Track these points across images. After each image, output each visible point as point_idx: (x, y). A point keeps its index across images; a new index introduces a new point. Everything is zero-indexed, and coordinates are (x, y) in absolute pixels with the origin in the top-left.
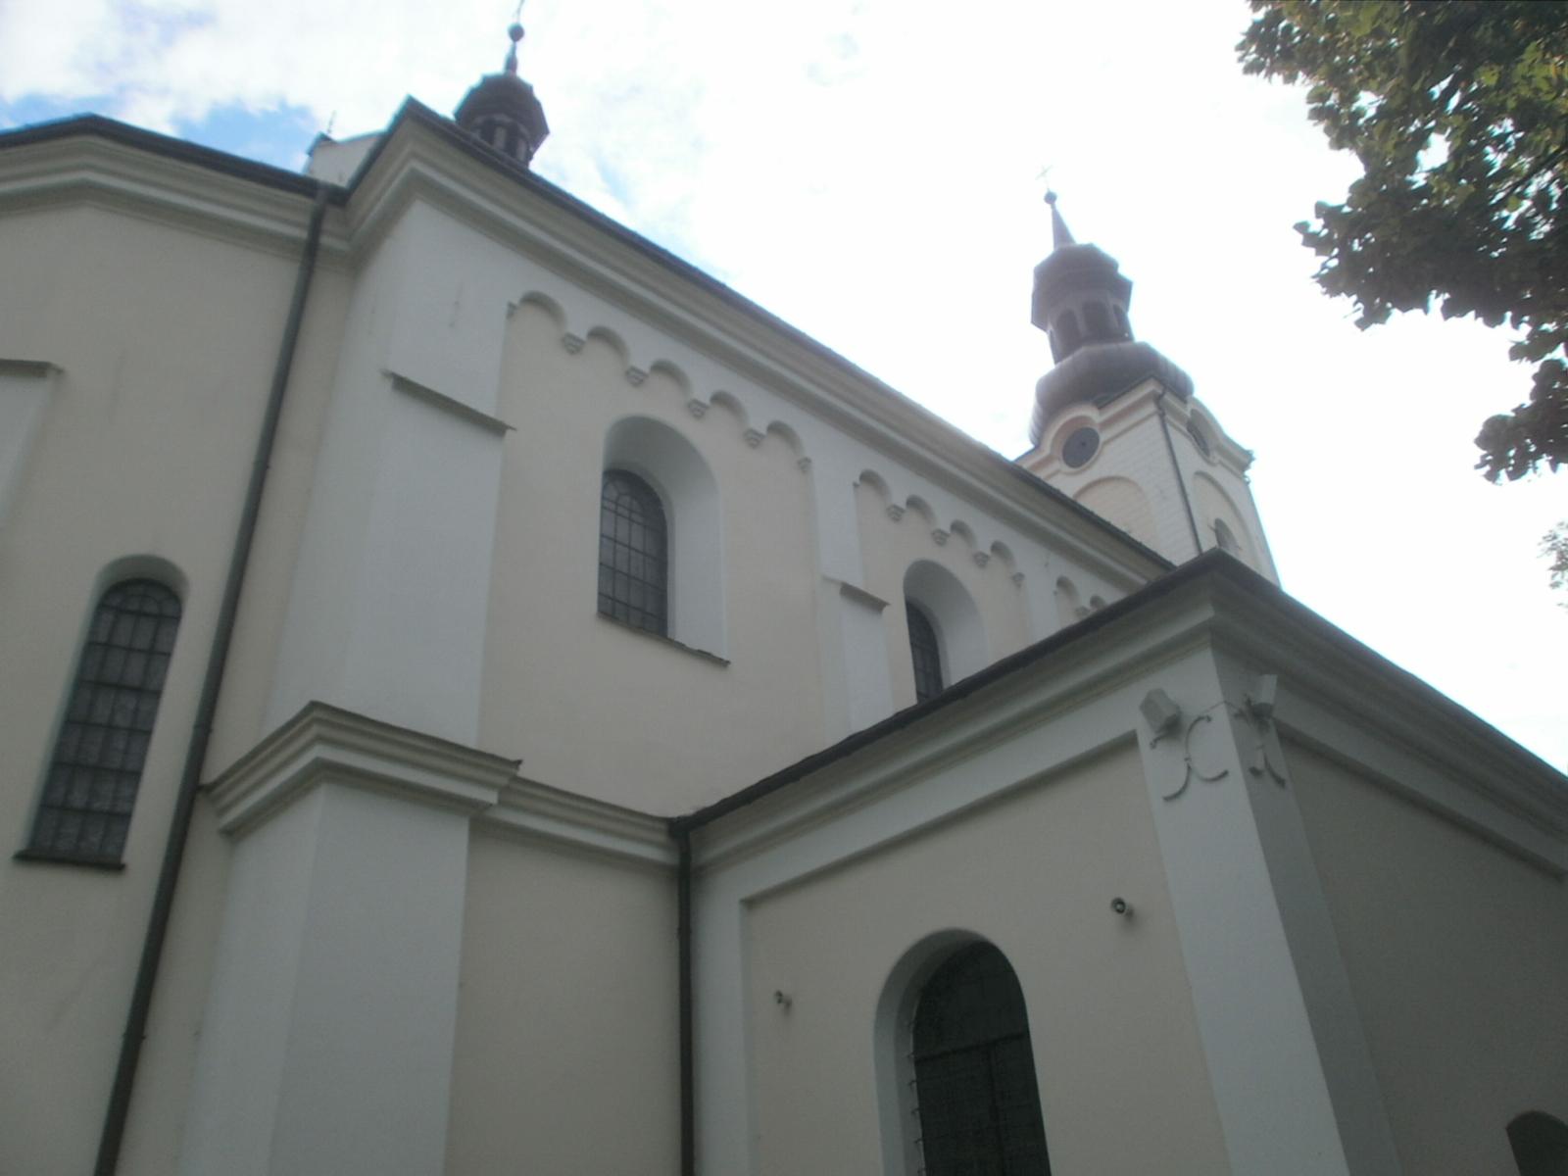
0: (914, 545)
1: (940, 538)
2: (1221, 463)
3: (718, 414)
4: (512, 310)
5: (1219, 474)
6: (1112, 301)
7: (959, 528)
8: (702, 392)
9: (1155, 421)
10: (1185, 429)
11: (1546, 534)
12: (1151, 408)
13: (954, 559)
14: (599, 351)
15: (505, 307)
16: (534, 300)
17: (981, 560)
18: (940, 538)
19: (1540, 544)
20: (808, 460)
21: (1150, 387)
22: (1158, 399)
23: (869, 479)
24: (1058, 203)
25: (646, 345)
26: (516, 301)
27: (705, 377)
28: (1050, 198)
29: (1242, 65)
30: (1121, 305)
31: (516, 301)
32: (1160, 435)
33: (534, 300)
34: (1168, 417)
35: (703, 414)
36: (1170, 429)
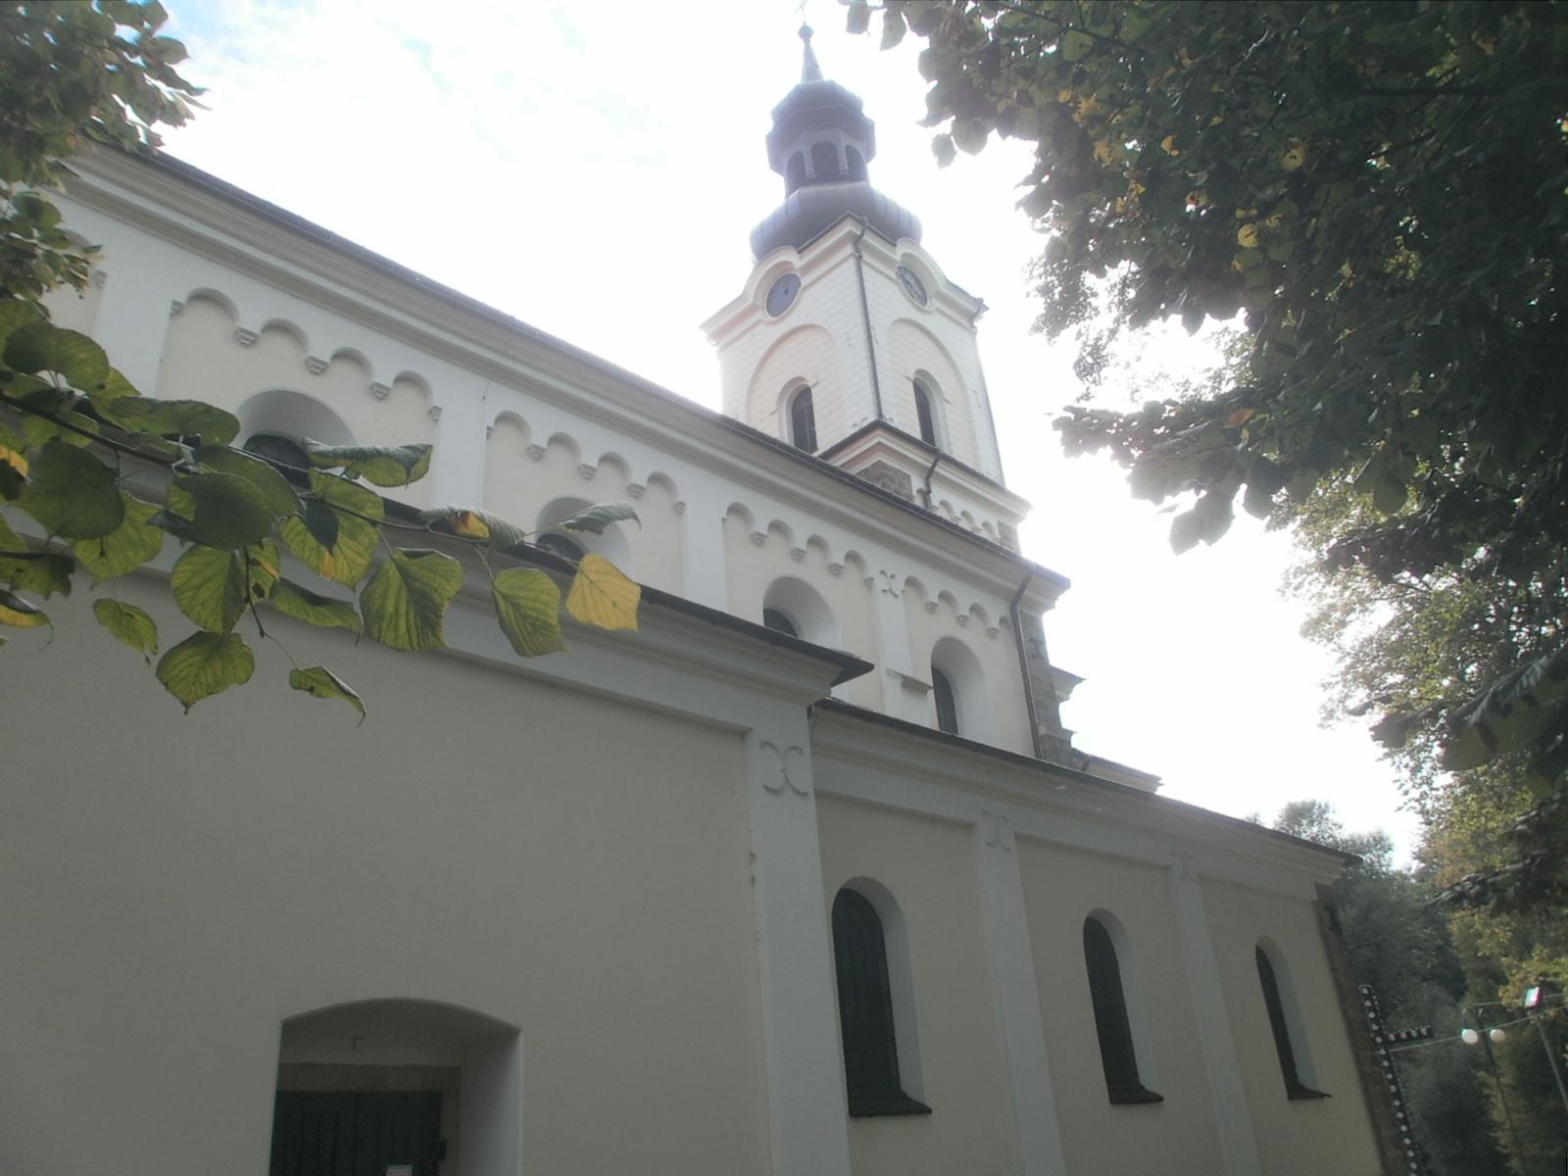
0: (773, 563)
1: (798, 555)
2: (938, 310)
3: (344, 370)
4: (177, 310)
5: (934, 323)
6: (844, 141)
7: (815, 542)
8: (322, 350)
9: (852, 262)
10: (894, 277)
11: (1318, 718)
12: (849, 249)
13: (811, 572)
14: (406, 394)
15: (485, 431)
16: (204, 297)
17: (836, 570)
18: (798, 555)
19: (1326, 686)
20: (683, 504)
21: (849, 227)
22: (857, 240)
23: (736, 510)
24: (813, 41)
25: (256, 304)
26: (182, 299)
27: (325, 334)
28: (806, 33)
29: (1317, 804)
30: (859, 147)
31: (182, 299)
32: (853, 278)
33: (204, 297)
34: (866, 257)
35: (592, 475)
36: (865, 269)
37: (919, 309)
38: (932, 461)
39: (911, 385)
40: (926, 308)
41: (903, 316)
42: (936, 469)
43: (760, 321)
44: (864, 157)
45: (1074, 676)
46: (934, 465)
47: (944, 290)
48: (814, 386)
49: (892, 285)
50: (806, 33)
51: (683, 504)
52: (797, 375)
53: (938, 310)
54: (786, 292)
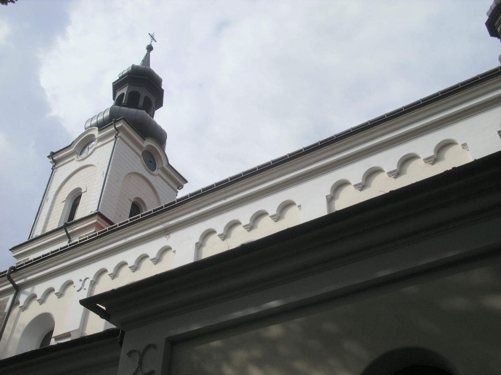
2: (159, 175)
28: (150, 48)
37: (149, 172)
38: (64, 231)
39: (131, 203)
40: (155, 172)
41: (137, 171)
42: (69, 232)
43: (74, 159)
44: (154, 104)
45: (122, 345)
46: (66, 232)
47: (165, 167)
48: (84, 192)
49: (139, 158)
50: (150, 48)
51: (175, 251)
52: (81, 187)
53: (159, 175)
54: (151, 162)
